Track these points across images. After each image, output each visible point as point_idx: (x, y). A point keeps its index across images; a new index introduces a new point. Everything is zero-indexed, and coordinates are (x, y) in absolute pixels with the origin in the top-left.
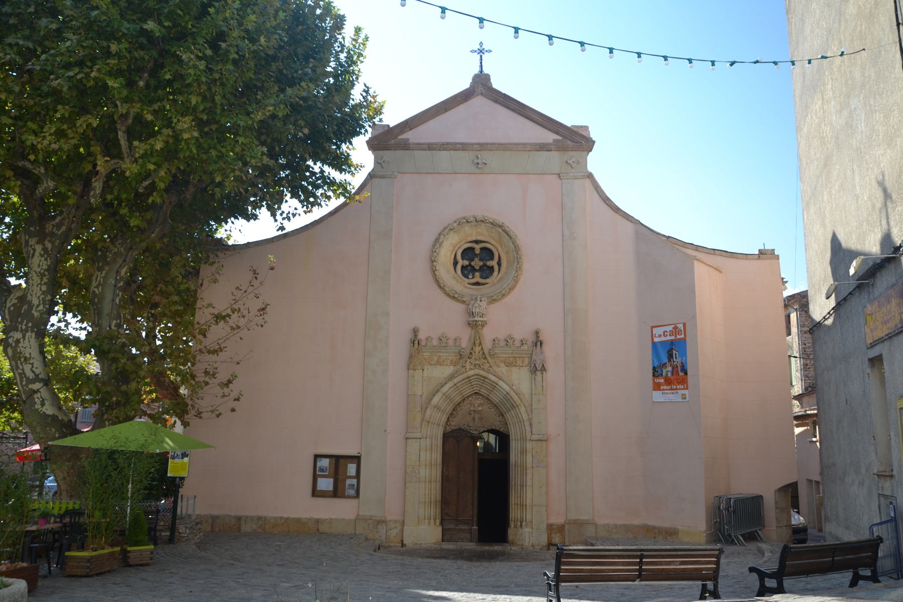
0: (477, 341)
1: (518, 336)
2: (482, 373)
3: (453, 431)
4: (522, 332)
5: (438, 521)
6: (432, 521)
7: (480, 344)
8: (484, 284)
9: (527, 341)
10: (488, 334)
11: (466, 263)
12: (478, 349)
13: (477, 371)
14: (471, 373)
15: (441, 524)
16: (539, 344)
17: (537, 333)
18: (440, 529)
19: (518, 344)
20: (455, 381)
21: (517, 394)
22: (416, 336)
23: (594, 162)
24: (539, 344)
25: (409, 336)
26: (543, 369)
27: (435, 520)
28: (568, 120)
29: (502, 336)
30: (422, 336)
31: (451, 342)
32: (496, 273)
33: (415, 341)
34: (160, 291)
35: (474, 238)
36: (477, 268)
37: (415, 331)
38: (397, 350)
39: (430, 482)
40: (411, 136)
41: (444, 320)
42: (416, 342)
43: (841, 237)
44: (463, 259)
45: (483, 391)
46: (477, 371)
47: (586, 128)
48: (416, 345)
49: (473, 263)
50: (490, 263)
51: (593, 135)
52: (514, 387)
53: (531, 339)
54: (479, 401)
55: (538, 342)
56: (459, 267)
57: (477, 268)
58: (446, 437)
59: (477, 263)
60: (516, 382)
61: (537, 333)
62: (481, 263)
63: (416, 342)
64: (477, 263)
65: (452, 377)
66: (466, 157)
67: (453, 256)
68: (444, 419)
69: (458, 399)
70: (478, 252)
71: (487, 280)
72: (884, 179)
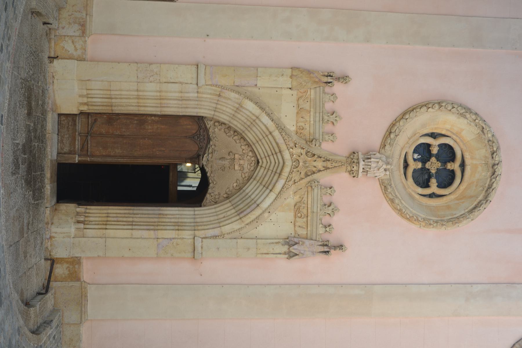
0: (330, 163)
1: (336, 220)
2: (287, 170)
3: (206, 130)
4: (342, 226)
5: (85, 108)
6: (85, 100)
7: (327, 168)
8: (405, 174)
10: (339, 179)
12: (320, 164)
13: (289, 163)
14: (287, 156)
15: (82, 113)
16: (326, 249)
18: (75, 111)
20: (276, 134)
21: (257, 218)
22: (338, 79)
24: (326, 249)
29: (337, 198)
30: (338, 87)
31: (328, 127)
32: (420, 190)
35: (468, 161)
36: (428, 165)
37: (344, 79)
39: (138, 98)
41: (360, 117)
44: (440, 146)
45: (261, 172)
46: (289, 163)
50: (434, 182)
52: (266, 215)
53: (333, 238)
55: (327, 248)
58: (199, 120)
59: (433, 165)
60: (273, 217)
61: (340, 247)
62: (433, 171)
64: (433, 165)
65: (281, 129)
67: (443, 132)
68: (224, 118)
69: (250, 137)
70: (449, 166)
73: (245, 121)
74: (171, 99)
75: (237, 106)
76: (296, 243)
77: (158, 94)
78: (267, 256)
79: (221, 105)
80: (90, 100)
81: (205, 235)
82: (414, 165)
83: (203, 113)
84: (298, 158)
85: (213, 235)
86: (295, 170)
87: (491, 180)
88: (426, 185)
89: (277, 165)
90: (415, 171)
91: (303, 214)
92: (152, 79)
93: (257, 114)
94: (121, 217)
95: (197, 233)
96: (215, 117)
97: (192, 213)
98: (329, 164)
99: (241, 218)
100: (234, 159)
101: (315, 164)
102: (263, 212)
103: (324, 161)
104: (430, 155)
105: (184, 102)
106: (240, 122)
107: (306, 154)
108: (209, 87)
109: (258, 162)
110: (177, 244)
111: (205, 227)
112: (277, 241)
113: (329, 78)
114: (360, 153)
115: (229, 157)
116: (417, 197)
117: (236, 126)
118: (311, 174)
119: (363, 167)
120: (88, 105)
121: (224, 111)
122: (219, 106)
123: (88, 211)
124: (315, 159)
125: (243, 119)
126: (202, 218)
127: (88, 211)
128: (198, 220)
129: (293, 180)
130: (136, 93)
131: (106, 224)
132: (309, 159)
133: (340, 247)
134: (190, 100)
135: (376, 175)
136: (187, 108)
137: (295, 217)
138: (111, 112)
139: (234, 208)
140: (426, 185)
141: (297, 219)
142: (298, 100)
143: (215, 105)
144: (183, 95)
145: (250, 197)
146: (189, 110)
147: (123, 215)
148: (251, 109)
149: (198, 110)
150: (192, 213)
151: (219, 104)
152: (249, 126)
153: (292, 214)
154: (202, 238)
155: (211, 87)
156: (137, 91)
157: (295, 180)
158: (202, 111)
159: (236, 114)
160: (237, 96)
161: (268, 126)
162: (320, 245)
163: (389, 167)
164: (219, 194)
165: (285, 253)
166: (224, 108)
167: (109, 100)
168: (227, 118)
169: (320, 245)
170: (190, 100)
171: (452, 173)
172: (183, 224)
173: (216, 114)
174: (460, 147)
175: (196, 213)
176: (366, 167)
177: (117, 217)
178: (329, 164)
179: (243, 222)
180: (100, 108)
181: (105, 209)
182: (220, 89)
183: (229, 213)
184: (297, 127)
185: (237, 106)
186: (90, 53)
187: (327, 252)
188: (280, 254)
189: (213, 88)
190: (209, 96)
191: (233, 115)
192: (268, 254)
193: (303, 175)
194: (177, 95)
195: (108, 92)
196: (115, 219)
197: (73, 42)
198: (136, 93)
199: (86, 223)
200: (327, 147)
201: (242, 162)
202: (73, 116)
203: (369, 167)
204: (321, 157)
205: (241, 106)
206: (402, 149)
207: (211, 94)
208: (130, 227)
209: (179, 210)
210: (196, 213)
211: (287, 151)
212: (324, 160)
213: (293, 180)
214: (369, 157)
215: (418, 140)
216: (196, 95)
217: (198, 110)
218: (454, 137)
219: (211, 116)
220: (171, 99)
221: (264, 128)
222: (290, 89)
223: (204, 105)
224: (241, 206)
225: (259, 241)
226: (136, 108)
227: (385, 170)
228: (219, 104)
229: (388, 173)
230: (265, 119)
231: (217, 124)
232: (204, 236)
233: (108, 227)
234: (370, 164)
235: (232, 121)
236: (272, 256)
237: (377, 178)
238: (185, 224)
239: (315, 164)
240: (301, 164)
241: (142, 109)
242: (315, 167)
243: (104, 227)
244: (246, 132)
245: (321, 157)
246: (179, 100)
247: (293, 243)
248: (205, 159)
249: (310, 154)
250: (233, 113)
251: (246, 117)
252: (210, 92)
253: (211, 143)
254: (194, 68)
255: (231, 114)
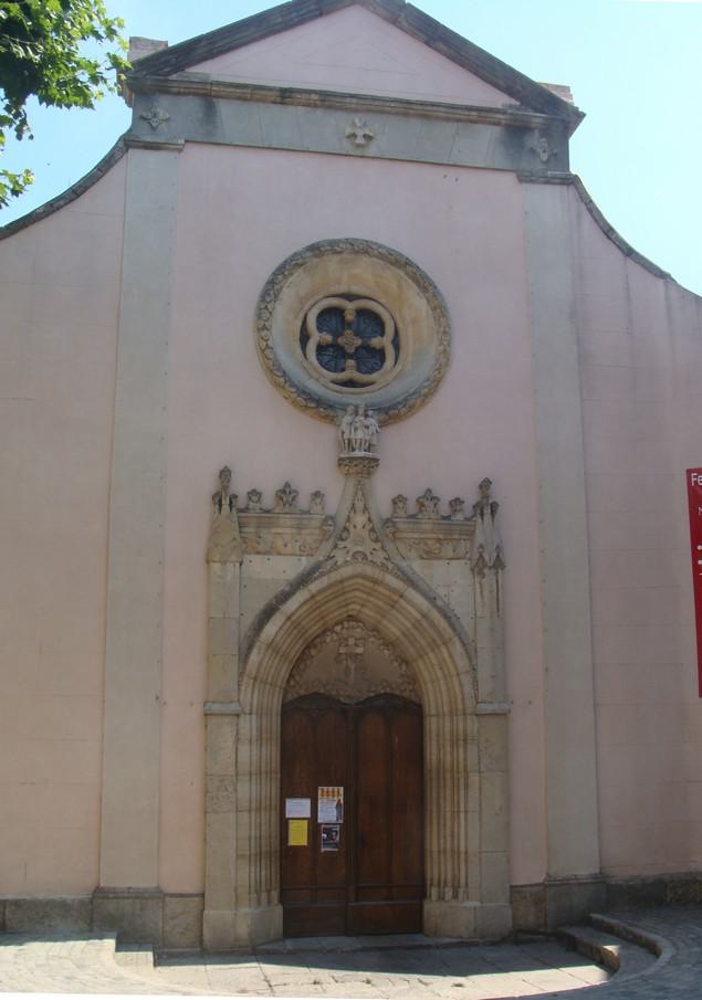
1: (446, 495)
2: (369, 570)
3: (302, 698)
4: (456, 483)
5: (275, 894)
6: (264, 895)
7: (366, 509)
8: (364, 385)
11: (328, 338)
12: (360, 519)
14: (347, 571)
15: (282, 900)
16: (487, 511)
18: (279, 910)
22: (225, 488)
23: (585, 153)
24: (487, 511)
25: (210, 485)
26: (499, 564)
27: (269, 891)
28: (537, 71)
29: (413, 493)
30: (240, 487)
31: (303, 501)
32: (389, 362)
33: (222, 498)
35: (343, 289)
36: (351, 350)
37: (225, 474)
38: (186, 520)
39: (259, 809)
40: (216, 70)
41: (283, 449)
42: (226, 503)
43: (90, 110)
44: (320, 329)
46: (360, 568)
47: (566, 89)
49: (340, 341)
50: (376, 342)
51: (578, 101)
52: (439, 603)
53: (471, 497)
54: (358, 632)
55: (487, 505)
56: (389, 329)
57: (351, 350)
58: (288, 710)
59: (351, 341)
60: (441, 591)
61: (485, 485)
62: (359, 342)
64: (351, 341)
65: (303, 580)
66: (334, 125)
67: (299, 323)
69: (315, 630)
70: (350, 317)
71: (374, 376)
73: (292, 637)
74: (260, 757)
76: (481, 556)
77: (254, 777)
80: (263, 888)
82: (351, 372)
84: (351, 554)
86: (370, 558)
87: (374, 256)
88: (380, 354)
90: (359, 370)
92: (231, 789)
94: (445, 830)
96: (284, 686)
98: (360, 505)
100: (346, 654)
101: (359, 526)
102: (435, 606)
103: (355, 512)
104: (334, 346)
110: (487, 741)
112: (478, 586)
114: (342, 456)
116: (399, 367)
120: (270, 891)
123: (435, 882)
124: (352, 526)
127: (435, 882)
130: (253, 813)
131: (459, 853)
133: (485, 485)
137: (439, 558)
138: (278, 854)
139: (427, 654)
140: (380, 354)
142: (258, 553)
143: (268, 686)
144: (254, 738)
147: (442, 827)
148: (276, 628)
149: (274, 713)
156: (250, 811)
160: (255, 650)
162: (482, 519)
164: (402, 676)
167: (263, 855)
169: (482, 519)
171: (361, 312)
174: (322, 299)
177: (445, 837)
178: (360, 505)
180: (273, 870)
181: (431, 857)
182: (245, 679)
183: (434, 662)
186: (191, 886)
189: (243, 688)
192: (498, 599)
193: (378, 546)
194: (254, 747)
195: (253, 857)
196: (449, 839)
197: (173, 919)
198: (253, 813)
199: (456, 884)
200: (335, 502)
202: (288, 916)
205: (271, 644)
206: (328, 388)
207: (253, 693)
208: (462, 816)
215: (311, 363)
216: (254, 716)
217: (274, 713)
218: (306, 307)
220: (260, 757)
225: (479, 614)
226: (273, 812)
227: (366, 416)
229: (370, 413)
231: (292, 683)
233: (462, 849)
239: (359, 526)
241: (273, 803)
243: (463, 856)
244: (307, 635)
246: (261, 744)
249: (345, 535)
254: (213, 721)
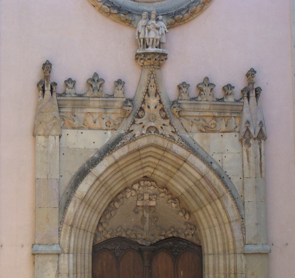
0: (153, 88)
1: (220, 82)
2: (160, 141)
3: (108, 241)
7: (157, 93)
9: (253, 77)
10: (171, 77)
12: (153, 101)
13: (154, 139)
14: (143, 142)
16: (252, 94)
17: (251, 74)
19: (219, 93)
20: (117, 154)
21: (220, 176)
22: (47, 78)
24: (252, 94)
25: (34, 75)
29: (194, 80)
30: (59, 76)
33: (46, 84)
34: (150, 264)
37: (47, 67)
42: (47, 89)
45: (159, 174)
48: (48, 92)
53: (240, 84)
55: (252, 91)
58: (97, 250)
60: (216, 157)
61: (251, 74)
63: (47, 89)
65: (109, 149)
68: (95, 220)
69: (118, 187)
72: (185, 118)
73: (100, 193)
75: (84, 204)
76: (248, 130)
78: (263, 164)
79: (81, 224)
81: (241, 240)
83: (89, 246)
84: (146, 128)
85: (240, 231)
86: (161, 131)
89: (153, 154)
91: (212, 122)
93: (94, 179)
95: (239, 251)
96: (94, 232)
97: (211, 257)
98: (152, 90)
99: (219, 198)
101: (152, 107)
103: (149, 96)
105: (79, 270)
106: (100, 199)
107: (140, 118)
108: (61, 238)
109: (146, 178)
111: (231, 240)
113: (46, 89)
114: (138, 51)
115: (141, 213)
117: (104, 205)
118: (164, 111)
119: (154, 47)
121: (87, 221)
122: (83, 226)
125: (98, 196)
126: (218, 245)
128: (221, 249)
129: (172, 134)
132: (146, 114)
134: (76, 262)
135: (164, 32)
136: (84, 266)
137: (214, 132)
139: (205, 206)
141: (218, 129)
143: (82, 232)
144: (71, 272)
145: (190, 187)
146: (87, 264)
150: (211, 257)
151: (81, 227)
152: (106, 189)
153: (212, 135)
154: (245, 244)
155: (62, 236)
157: (172, 132)
158: (87, 247)
159: (92, 204)
160: (72, 204)
161: (108, 165)
163: (153, 16)
164: (186, 223)
165: (260, 144)
166: (85, 219)
168: (96, 215)
170: (76, 262)
172: (228, 268)
173: (90, 230)
175: (210, 251)
176: (155, 43)
179: (224, 195)
182: (64, 226)
184: (107, 130)
185: (84, 204)
187: (258, 92)
188: (260, 150)
189: (62, 233)
190: (72, 239)
191: (93, 208)
193: (167, 122)
201: (146, 197)
203: (155, 41)
204: (144, 100)
209: (208, 274)
210: (210, 251)
211: (139, 141)
212: (147, 96)
213: (172, 134)
214: (142, 40)
216: (71, 255)
217: (87, 252)
219: (93, 235)
221: (110, 171)
222: (60, 137)
223: (82, 246)
224: (202, 197)
227: (157, 20)
228: (81, 227)
229: (160, 17)
230: (100, 168)
232: (242, 243)
234: (151, 40)
235: (98, 210)
236: (262, 158)
237: (167, 31)
238: (227, 266)
239: (152, 107)
240: (153, 124)
242: (156, 107)
245: (144, 100)
247: (248, 133)
248: (144, 243)
249: (140, 113)
250: (90, 208)
251: (96, 192)
252: (67, 238)
253: (124, 235)
254: (39, 259)
255: (91, 211)
